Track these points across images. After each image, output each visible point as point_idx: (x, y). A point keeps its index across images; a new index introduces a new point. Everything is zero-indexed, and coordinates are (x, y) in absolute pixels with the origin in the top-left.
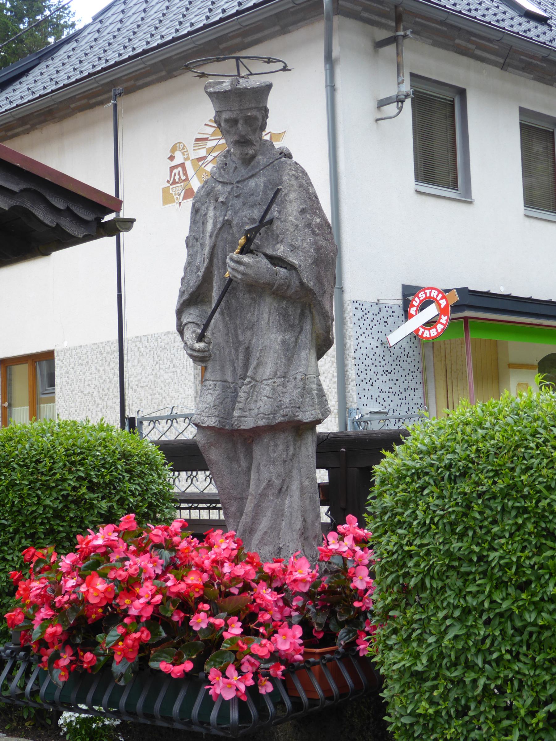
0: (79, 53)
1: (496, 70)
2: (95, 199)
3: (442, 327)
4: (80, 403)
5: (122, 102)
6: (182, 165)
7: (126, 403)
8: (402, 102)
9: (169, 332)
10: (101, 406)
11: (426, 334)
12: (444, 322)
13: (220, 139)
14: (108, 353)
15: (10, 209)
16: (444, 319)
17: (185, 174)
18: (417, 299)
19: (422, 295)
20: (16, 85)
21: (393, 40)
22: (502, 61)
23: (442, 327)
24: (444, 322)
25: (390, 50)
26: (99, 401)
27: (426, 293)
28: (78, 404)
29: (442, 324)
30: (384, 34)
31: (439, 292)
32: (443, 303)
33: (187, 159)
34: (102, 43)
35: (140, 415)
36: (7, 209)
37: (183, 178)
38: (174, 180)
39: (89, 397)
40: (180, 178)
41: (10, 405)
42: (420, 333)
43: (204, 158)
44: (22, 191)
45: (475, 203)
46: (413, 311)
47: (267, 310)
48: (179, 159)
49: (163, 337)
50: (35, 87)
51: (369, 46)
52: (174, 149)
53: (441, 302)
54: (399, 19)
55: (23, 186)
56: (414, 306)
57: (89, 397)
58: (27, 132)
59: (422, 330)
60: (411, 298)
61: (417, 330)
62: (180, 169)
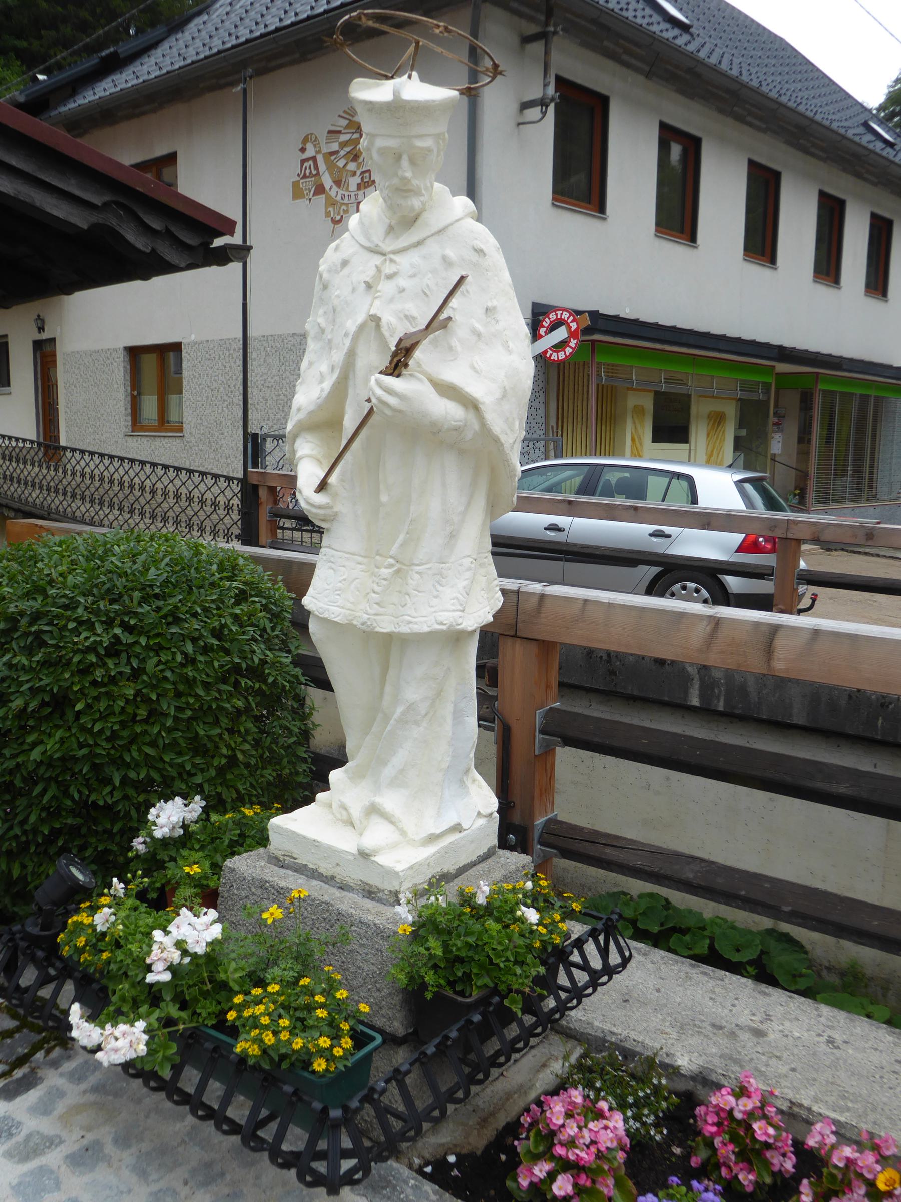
0: (210, 27)
1: (641, 78)
2: (201, 218)
3: (571, 350)
4: (207, 397)
5: (252, 85)
6: (314, 159)
7: (250, 401)
8: (547, 107)
9: (295, 334)
10: (227, 403)
11: (554, 356)
12: (573, 346)
13: (353, 133)
14: (235, 349)
15: (89, 228)
16: (573, 343)
17: (317, 168)
18: (547, 319)
19: (553, 316)
20: (145, 59)
21: (543, 36)
22: (647, 68)
23: (571, 350)
24: (573, 346)
25: (537, 47)
26: (225, 397)
27: (556, 314)
28: (204, 399)
29: (571, 347)
30: (532, 29)
31: (570, 314)
32: (574, 326)
33: (319, 152)
34: (234, 17)
35: (265, 431)
36: (85, 227)
37: (314, 172)
38: (305, 173)
39: (215, 392)
40: (311, 172)
41: (139, 394)
42: (548, 355)
43: (337, 152)
44: (105, 204)
45: (609, 220)
46: (542, 331)
47: (462, 584)
48: (310, 152)
49: (290, 339)
50: (163, 62)
51: (515, 40)
52: (305, 140)
53: (571, 324)
54: (549, 13)
55: (107, 198)
56: (544, 326)
57: (215, 392)
58: (154, 111)
59: (550, 352)
60: (541, 317)
61: (546, 352)
62: (311, 162)
